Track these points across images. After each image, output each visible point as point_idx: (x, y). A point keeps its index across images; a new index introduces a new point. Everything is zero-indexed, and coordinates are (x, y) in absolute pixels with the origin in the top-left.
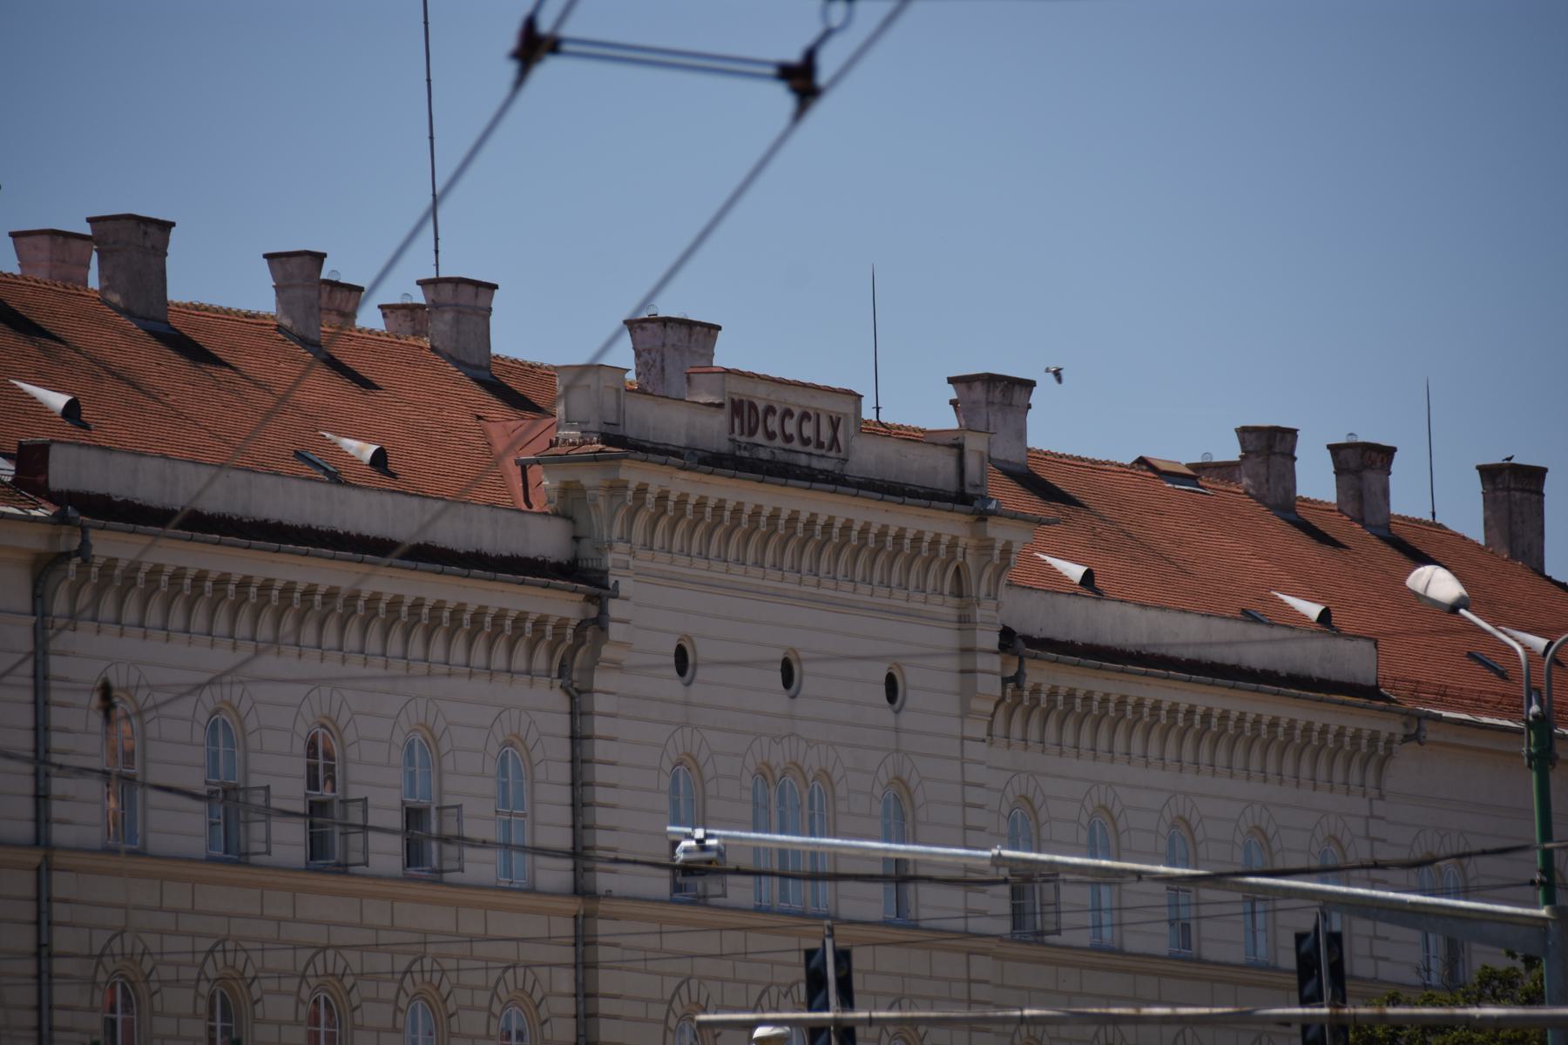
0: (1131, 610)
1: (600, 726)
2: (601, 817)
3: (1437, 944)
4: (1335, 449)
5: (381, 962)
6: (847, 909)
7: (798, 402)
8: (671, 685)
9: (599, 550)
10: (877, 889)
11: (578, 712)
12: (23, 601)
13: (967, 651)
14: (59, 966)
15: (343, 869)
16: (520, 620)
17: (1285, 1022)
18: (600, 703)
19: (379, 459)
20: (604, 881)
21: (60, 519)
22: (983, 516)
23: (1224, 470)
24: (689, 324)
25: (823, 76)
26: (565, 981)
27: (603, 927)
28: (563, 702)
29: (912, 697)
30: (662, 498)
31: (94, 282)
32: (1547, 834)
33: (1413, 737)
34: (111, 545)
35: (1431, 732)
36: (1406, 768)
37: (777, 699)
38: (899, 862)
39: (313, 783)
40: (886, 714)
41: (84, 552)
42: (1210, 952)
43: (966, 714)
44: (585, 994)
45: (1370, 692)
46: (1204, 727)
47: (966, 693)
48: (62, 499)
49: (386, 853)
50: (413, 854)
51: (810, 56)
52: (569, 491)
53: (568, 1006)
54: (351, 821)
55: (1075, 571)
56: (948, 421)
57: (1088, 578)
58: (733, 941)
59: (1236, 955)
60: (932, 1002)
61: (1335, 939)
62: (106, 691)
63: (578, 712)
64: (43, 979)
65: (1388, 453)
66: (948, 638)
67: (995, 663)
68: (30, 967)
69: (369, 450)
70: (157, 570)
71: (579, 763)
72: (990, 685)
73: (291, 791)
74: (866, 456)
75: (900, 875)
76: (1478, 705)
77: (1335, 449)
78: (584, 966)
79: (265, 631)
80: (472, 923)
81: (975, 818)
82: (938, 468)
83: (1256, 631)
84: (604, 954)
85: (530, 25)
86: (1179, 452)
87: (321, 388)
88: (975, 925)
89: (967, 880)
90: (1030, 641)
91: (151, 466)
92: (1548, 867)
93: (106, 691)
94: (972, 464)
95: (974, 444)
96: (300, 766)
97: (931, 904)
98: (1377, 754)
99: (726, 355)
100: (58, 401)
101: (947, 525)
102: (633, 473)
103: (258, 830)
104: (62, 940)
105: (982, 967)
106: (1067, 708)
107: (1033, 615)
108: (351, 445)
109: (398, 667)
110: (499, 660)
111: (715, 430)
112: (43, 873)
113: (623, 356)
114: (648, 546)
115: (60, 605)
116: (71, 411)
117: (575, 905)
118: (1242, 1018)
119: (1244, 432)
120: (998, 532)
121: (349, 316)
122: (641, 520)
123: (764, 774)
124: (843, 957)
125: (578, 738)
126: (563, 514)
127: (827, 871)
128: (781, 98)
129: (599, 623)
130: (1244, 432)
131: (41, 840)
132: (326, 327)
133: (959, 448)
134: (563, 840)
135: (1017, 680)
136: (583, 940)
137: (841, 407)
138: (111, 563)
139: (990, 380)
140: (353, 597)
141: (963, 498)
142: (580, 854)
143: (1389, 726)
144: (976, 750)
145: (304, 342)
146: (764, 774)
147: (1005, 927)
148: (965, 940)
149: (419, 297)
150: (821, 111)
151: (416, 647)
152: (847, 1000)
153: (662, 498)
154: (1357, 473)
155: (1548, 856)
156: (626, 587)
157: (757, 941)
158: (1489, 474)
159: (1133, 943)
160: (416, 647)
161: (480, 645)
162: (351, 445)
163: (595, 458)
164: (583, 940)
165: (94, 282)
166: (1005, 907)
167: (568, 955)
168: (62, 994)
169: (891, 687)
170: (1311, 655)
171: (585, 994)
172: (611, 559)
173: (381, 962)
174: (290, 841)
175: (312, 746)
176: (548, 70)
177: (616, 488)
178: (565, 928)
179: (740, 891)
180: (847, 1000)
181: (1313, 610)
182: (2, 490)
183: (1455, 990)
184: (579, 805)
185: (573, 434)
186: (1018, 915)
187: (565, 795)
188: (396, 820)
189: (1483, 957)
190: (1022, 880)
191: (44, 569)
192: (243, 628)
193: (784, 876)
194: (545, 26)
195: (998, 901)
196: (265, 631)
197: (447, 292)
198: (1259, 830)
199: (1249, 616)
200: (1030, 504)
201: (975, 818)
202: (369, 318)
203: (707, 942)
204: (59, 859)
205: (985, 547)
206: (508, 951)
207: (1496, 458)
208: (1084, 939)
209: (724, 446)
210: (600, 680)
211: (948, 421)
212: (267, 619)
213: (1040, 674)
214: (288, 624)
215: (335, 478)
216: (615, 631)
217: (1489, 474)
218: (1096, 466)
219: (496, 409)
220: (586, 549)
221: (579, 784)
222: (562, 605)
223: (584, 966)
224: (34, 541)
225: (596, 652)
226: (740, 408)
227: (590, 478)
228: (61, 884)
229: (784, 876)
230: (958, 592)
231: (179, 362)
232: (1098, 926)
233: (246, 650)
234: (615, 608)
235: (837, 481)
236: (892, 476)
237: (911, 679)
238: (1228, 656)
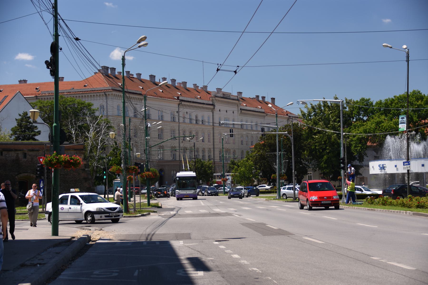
0: (249, 107)
1: (214, 115)
2: (214, 121)
3: (268, 128)
4: (262, 97)
5: (200, 130)
6: (230, 127)
7: (227, 94)
8: (219, 112)
9: (214, 103)
10: (232, 125)
11: (213, 114)
12: (178, 106)
13: (238, 110)
14: (180, 130)
15: (198, 124)
16: (196, 106)
17: (261, 134)
18: (214, 113)
19: (200, 97)
20: (214, 125)
21: (180, 101)
22: (239, 101)
23: (255, 98)
24: (220, 89)
25: (237, 72)
26: (212, 131)
27: (215, 128)
28: (212, 113)
29: (235, 113)
30: (218, 100)
31: (182, 86)
32: (277, 122)
33: (267, 115)
34: (183, 103)
35: (268, 115)
36: (266, 117)
37: (226, 113)
38: (234, 123)
39: (196, 118)
40: (233, 114)
41: (181, 103)
42: (253, 129)
43: (238, 114)
44: (213, 132)
45: (264, 113)
46: (253, 115)
47: (238, 113)
48: (180, 100)
49: (201, 123)
50: (202, 123)
51: (236, 70)
52: (212, 99)
53: (212, 133)
54: (207, 123)
55: (245, 105)
56: (237, 95)
57: (246, 105)
58: (223, 129)
59: (255, 130)
60: (236, 133)
61: (264, 128)
62: (187, 112)
63: (213, 114)
64: (179, 131)
65: (265, 97)
66: (237, 109)
67: (240, 111)
68: (178, 130)
69: (200, 97)
70: (190, 105)
71: (213, 117)
72: (240, 112)
73: (195, 119)
74: (232, 97)
75: (234, 124)
76: (271, 113)
77: (262, 97)
78: (213, 130)
79: (184, 107)
80: (206, 127)
81: (238, 121)
82: (236, 98)
83: (257, 109)
84: (215, 129)
85: (218, 68)
86: (252, 97)
87: (197, 93)
88: (239, 128)
89: (238, 125)
90: (242, 109)
91: (186, 98)
92: (277, 124)
93: (187, 112)
94: (238, 98)
95: (239, 96)
96: (195, 117)
97: (236, 126)
98: (264, 117)
99: (222, 90)
100: (180, 94)
101: (237, 102)
102: (217, 98)
103: (199, 122)
104: (180, 128)
105: (239, 130)
106: (245, 114)
107: (242, 108)
108: (198, 96)
109: (201, 111)
110: (208, 111)
111: (222, 96)
112: (179, 124)
113: (216, 90)
114: (217, 103)
115: (180, 107)
116: (181, 94)
117: (213, 126)
118: (258, 133)
119: (256, 96)
120: (240, 102)
121: (198, 88)
122: (217, 101)
123: (225, 118)
124: (232, 130)
125: (213, 115)
126: (212, 101)
127: (420, 161)
128: (234, 73)
129: (214, 108)
130: (256, 96)
131: (179, 122)
132: (197, 89)
133: (238, 97)
134: (212, 122)
135: (241, 112)
136: (213, 128)
137: (230, 94)
138: (183, 104)
139: (240, 92)
140: (203, 107)
141: (238, 100)
142: (213, 123)
143: (265, 115)
144: (239, 116)
145: (195, 90)
146: (225, 118)
147: (240, 128)
148: (238, 129)
149: (203, 87)
150: (237, 74)
151: (203, 110)
152: (232, 132)
153: (218, 100)
154: (263, 98)
155: (277, 123)
156: (216, 106)
157: (224, 129)
158: (271, 98)
159: (249, 129)
160: (203, 110)
161: (203, 109)
162: (198, 96)
163: (214, 97)
164: (213, 128)
165: (182, 86)
166: (240, 126)
167: (212, 129)
168: (180, 132)
169: (233, 112)
170: (260, 110)
171: (213, 132)
172: (215, 104)
173: (200, 130)
174: (194, 122)
175: (196, 116)
176: (219, 71)
177: (215, 99)
178: (212, 128)
179: (223, 125)
180: (232, 132)
181: (260, 107)
182: (426, 121)
183: (269, 132)
184: (213, 120)
185: (213, 96)
186: (241, 127)
187: (212, 119)
188: (201, 121)
189: (271, 129)
190: (241, 125)
191: (179, 104)
192: (183, 107)
193: (226, 124)
194: (219, 69)
195: (240, 126)
196: (184, 107)
197: (205, 87)
198: (257, 121)
199: (256, 108)
200: (242, 100)
201: (238, 121)
202: (199, 88)
203: (221, 129)
204: (180, 123)
205: (239, 103)
206: (208, 129)
207: (272, 97)
208: (245, 128)
209: (222, 97)
210: (214, 112)
211: (237, 95)
212: (134, 100)
213: (243, 111)
214: (189, 107)
215: (197, 99)
216: (215, 109)
217: (271, 98)
218: (246, 98)
219: (208, 94)
220: (214, 103)
221: (213, 118)
222: (212, 107)
223: (213, 130)
224: (178, 103)
225: (214, 110)
226: (223, 94)
227: (214, 99)
228: (180, 125)
229: (226, 124)
230: (238, 106)
231: (187, 91)
232: (246, 127)
233: (183, 109)
234: (215, 107)
235: (230, 99)
236: (233, 98)
237: (234, 112)
238: (255, 110)
